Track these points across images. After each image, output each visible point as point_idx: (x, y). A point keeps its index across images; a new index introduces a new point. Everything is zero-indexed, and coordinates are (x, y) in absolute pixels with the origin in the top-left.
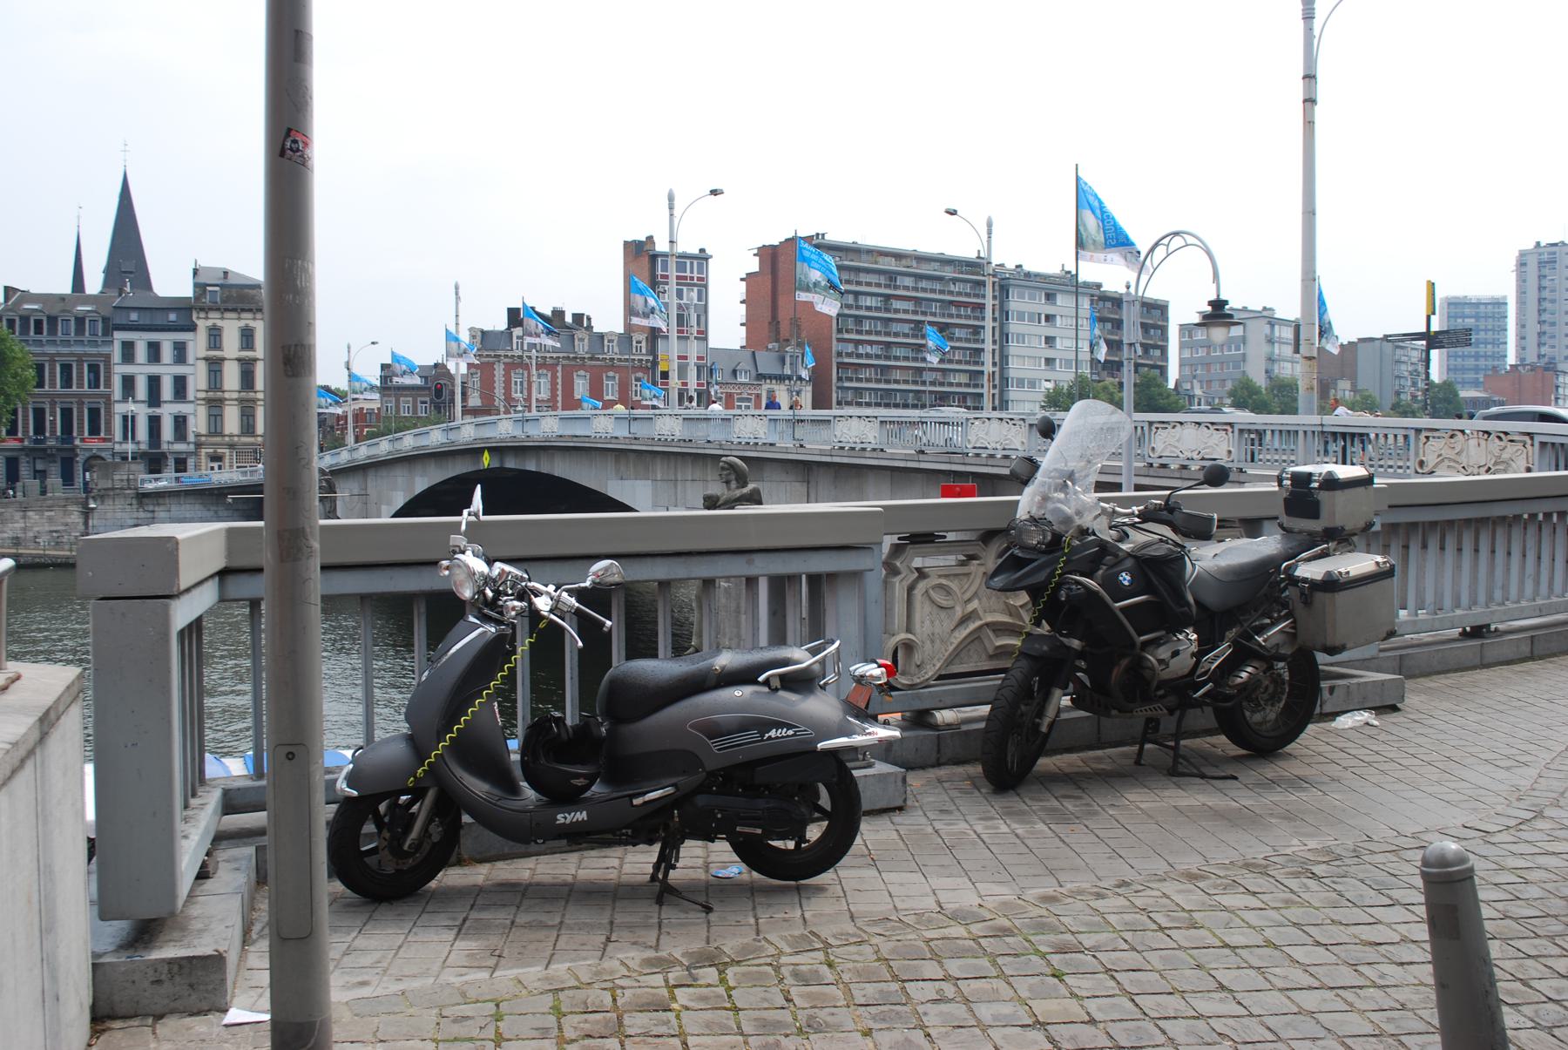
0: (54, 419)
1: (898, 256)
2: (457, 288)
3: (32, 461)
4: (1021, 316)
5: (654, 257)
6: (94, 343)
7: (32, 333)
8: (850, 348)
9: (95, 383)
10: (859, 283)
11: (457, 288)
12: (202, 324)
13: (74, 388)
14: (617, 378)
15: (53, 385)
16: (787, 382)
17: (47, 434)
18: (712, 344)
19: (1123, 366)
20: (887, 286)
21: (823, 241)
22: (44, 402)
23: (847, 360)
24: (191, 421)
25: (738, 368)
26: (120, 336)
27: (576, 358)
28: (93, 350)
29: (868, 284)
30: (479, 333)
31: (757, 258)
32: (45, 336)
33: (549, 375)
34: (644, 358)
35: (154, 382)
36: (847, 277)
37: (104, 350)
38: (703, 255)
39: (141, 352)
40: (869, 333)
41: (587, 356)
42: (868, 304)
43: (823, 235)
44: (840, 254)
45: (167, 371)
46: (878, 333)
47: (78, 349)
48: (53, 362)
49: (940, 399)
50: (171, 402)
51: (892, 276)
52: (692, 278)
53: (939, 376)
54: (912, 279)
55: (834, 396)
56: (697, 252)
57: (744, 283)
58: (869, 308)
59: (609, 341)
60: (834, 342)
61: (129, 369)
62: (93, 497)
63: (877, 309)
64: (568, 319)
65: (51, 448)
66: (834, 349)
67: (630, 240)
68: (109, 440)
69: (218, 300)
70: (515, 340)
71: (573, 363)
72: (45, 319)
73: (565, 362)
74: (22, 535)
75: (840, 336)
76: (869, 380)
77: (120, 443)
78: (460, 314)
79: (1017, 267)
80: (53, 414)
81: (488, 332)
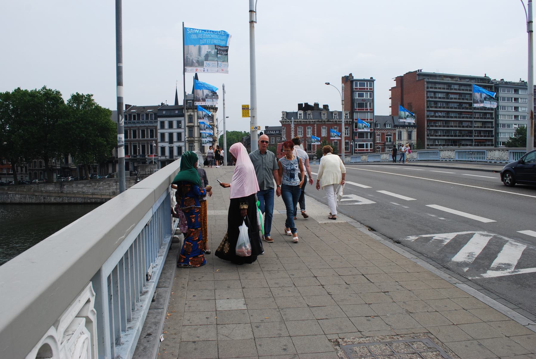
0: (140, 149)
1: (452, 77)
2: (223, 87)
3: (133, 163)
4: (504, 99)
5: (352, 82)
6: (151, 122)
7: (132, 120)
8: (432, 114)
9: (152, 136)
10: (436, 88)
11: (223, 87)
12: (187, 114)
13: (146, 138)
15: (139, 137)
16: (406, 128)
17: (137, 154)
19: (204, 163)
20: (447, 89)
21: (421, 73)
22: (145, 143)
23: (431, 119)
24: (183, 148)
25: (386, 123)
26: (159, 119)
27: (322, 121)
28: (151, 125)
29: (440, 88)
30: (285, 113)
31: (395, 81)
32: (136, 121)
33: (312, 128)
34: (349, 120)
35: (171, 135)
36: (431, 86)
37: (155, 124)
38: (372, 80)
39: (166, 125)
40: (440, 107)
41: (326, 120)
42: (440, 96)
43: (421, 70)
44: (428, 77)
45: (175, 131)
46: (444, 108)
47: (147, 125)
48: (139, 129)
49: (470, 133)
50: (176, 142)
51: (449, 85)
52: (367, 89)
53: (469, 124)
54: (458, 86)
55: (426, 133)
57: (391, 91)
58: (440, 98)
59: (335, 114)
60: (426, 112)
61: (162, 131)
62: (139, 177)
63: (443, 98)
64: (321, 106)
65: (138, 159)
66: (426, 115)
67: (343, 76)
68: (157, 156)
69: (192, 105)
70: (307, 116)
71: (321, 123)
72: (136, 115)
73: (318, 123)
74: (116, 191)
75: (428, 109)
76: (440, 126)
77: (160, 157)
78: (225, 99)
79: (501, 80)
80: (139, 147)
81: (288, 113)
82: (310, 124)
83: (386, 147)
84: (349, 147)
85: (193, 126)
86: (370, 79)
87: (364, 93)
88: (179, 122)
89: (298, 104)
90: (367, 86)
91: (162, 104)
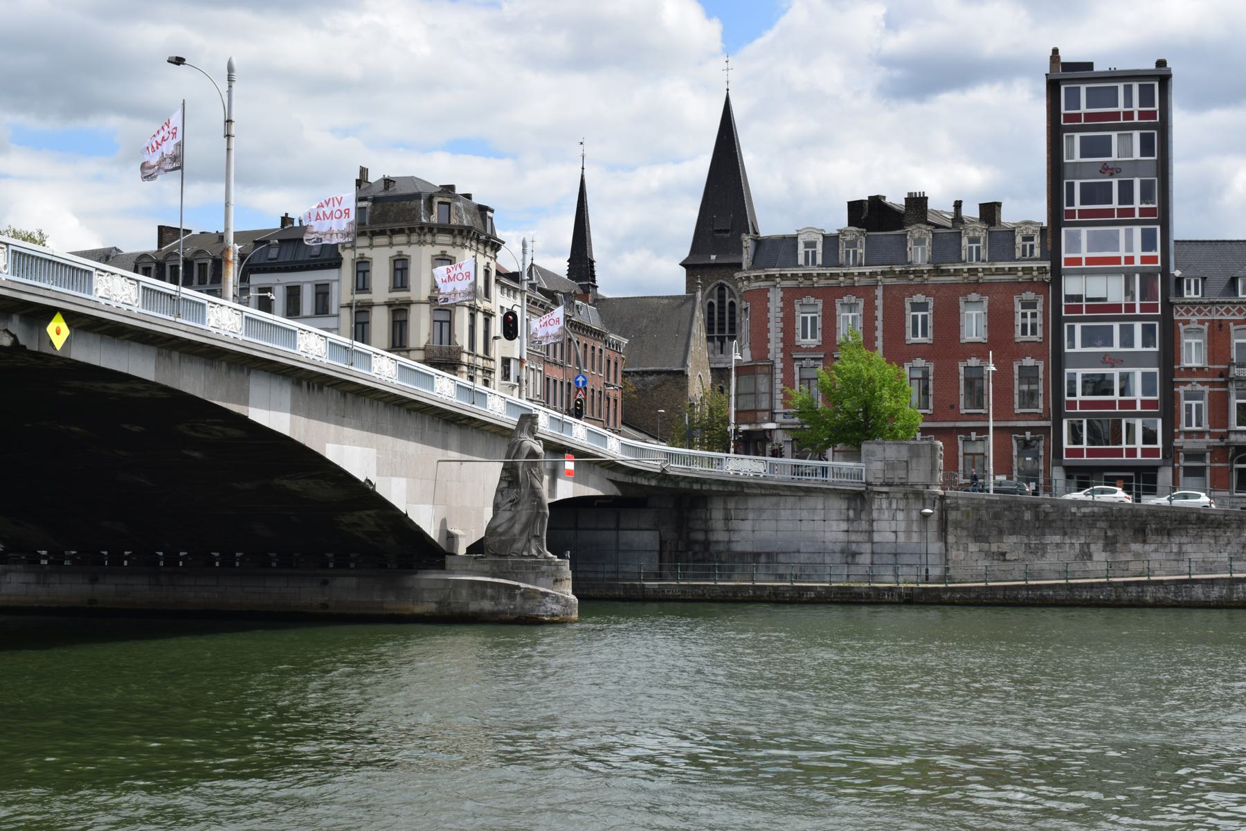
14: (931, 306)
18: (1184, 226)
33: (861, 303)
34: (1035, 265)
56: (1153, 66)
73: (888, 281)
82: (851, 289)
83: (1232, 388)
84: (1041, 392)
85: (370, 305)
86: (1153, 67)
87: (1114, 135)
88: (322, 293)
89: (849, 203)
90: (1128, 102)
91: (286, 220)
